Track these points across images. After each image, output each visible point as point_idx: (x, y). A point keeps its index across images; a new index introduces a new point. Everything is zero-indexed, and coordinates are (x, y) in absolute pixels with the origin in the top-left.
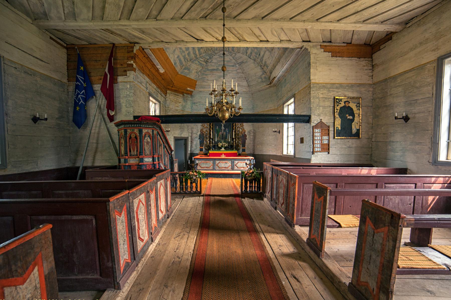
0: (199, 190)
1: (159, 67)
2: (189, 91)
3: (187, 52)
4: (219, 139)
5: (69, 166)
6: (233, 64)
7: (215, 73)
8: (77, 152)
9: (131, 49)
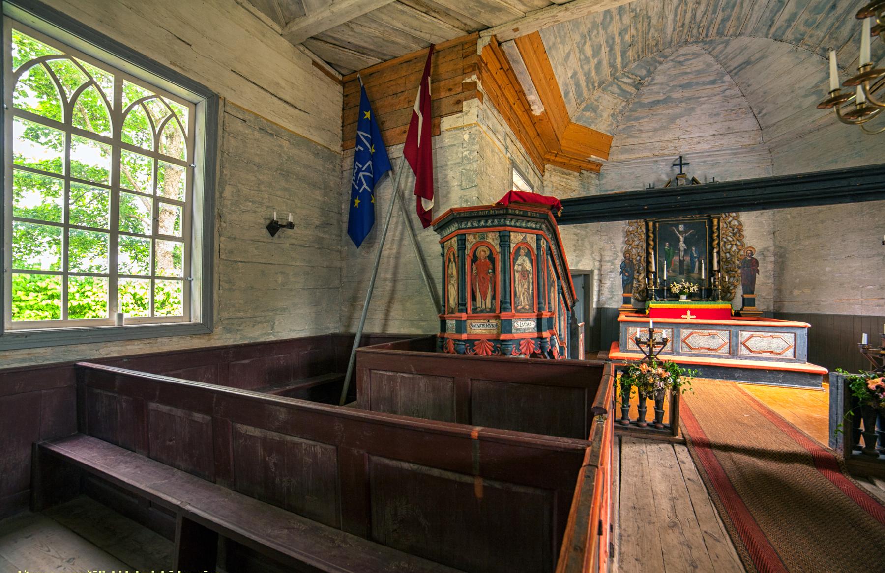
0: (666, 420)
1: (532, 97)
2: (593, 163)
3: (596, 61)
4: (671, 274)
5: (337, 331)
6: (712, 78)
7: (659, 112)
8: (353, 301)
9: (471, 49)
